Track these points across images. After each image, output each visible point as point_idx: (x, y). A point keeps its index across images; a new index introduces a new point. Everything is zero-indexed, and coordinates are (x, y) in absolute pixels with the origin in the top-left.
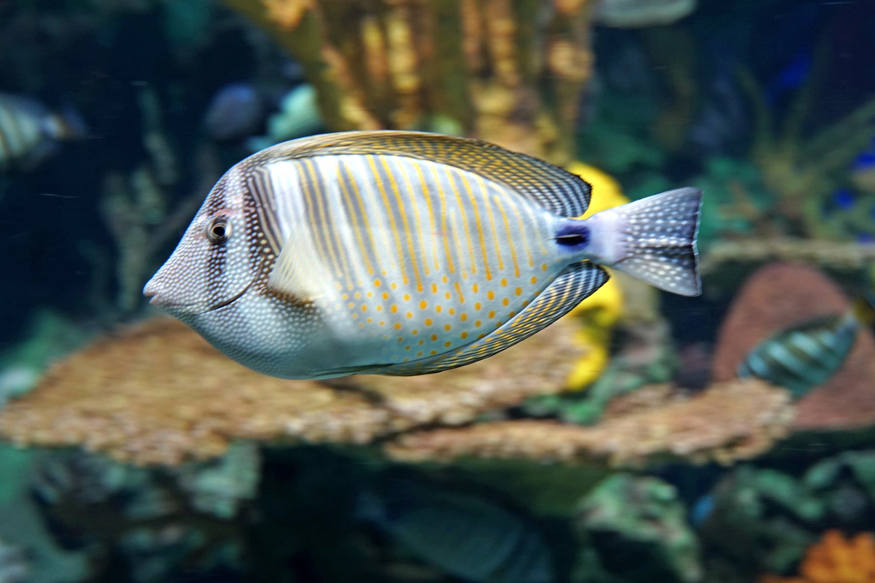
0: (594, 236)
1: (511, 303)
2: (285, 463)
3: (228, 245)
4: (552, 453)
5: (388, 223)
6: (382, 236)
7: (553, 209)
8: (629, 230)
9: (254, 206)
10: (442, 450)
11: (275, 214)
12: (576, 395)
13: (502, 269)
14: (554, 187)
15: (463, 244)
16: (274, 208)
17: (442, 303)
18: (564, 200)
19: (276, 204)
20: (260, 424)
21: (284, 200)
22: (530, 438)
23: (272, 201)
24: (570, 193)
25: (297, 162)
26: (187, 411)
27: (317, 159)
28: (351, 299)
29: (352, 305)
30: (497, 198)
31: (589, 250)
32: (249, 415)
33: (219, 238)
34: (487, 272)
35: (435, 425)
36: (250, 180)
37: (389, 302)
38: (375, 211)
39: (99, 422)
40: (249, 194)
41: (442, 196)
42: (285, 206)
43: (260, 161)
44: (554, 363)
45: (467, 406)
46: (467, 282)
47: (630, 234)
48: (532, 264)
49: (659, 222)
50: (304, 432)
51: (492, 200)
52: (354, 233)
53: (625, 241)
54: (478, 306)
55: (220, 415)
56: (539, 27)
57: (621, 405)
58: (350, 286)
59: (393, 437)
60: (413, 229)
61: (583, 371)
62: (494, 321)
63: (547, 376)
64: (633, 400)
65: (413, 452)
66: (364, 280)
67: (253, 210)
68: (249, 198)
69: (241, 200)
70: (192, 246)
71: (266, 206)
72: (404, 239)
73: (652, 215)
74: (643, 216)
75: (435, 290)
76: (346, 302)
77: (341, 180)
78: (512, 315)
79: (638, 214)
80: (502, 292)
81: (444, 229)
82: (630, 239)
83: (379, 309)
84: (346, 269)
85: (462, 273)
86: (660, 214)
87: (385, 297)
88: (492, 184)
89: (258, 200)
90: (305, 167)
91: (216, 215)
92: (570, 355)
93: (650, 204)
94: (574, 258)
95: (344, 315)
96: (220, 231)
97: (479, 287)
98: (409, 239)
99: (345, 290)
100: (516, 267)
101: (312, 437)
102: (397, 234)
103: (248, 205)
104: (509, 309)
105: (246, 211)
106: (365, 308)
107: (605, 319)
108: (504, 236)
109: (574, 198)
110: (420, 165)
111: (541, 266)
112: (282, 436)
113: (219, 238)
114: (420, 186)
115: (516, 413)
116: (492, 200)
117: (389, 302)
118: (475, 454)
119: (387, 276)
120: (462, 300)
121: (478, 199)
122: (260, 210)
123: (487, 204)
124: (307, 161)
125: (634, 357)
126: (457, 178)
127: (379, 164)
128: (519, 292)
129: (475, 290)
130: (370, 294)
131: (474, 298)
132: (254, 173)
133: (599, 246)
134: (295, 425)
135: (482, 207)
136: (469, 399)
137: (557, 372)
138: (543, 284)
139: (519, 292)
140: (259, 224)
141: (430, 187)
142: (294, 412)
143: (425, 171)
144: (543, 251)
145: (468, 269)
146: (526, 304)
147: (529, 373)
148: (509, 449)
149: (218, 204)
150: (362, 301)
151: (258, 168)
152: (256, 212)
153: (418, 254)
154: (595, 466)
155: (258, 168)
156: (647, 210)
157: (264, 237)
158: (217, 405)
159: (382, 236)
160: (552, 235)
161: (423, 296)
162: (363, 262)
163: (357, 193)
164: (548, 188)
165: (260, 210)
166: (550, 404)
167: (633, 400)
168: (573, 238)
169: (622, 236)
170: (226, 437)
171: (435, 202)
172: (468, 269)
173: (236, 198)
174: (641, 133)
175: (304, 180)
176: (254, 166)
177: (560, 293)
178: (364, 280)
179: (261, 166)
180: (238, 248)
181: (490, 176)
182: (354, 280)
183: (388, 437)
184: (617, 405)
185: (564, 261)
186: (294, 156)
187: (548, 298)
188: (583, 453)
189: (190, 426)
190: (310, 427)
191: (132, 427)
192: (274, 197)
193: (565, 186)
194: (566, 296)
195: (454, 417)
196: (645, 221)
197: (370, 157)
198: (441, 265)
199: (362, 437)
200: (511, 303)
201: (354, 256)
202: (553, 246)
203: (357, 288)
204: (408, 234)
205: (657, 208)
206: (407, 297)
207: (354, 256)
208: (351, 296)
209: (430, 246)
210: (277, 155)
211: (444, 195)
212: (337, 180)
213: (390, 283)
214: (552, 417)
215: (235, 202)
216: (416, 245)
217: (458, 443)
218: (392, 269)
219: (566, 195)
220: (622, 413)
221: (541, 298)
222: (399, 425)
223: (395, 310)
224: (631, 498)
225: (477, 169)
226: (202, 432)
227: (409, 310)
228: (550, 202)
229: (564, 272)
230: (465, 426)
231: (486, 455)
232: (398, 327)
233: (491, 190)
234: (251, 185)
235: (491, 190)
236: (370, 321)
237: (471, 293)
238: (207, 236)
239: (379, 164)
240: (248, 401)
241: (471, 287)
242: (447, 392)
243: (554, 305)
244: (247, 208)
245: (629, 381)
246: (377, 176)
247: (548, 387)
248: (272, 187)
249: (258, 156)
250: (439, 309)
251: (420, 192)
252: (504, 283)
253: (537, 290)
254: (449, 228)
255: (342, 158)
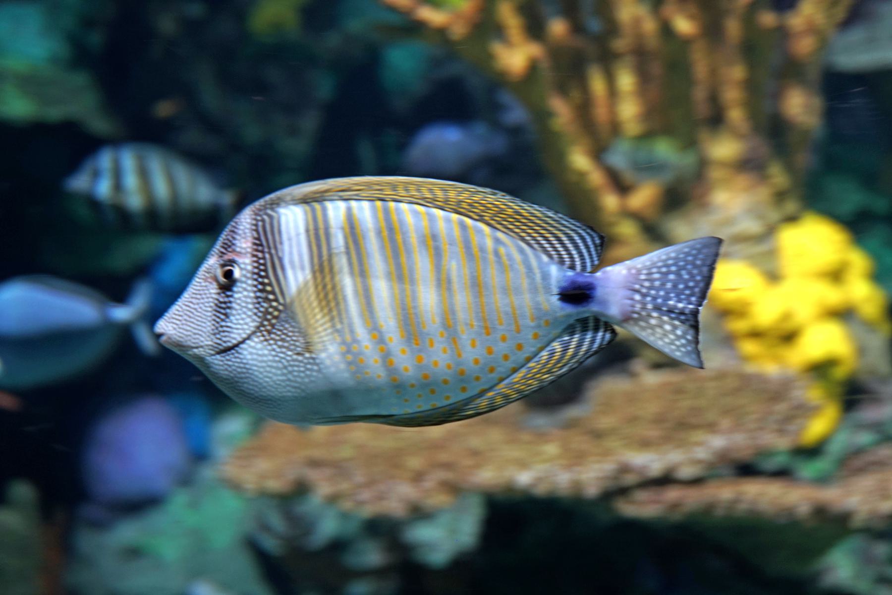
0: (599, 292)
1: (512, 358)
2: (510, 516)
3: (235, 289)
4: (789, 512)
5: (389, 276)
6: (381, 288)
7: (561, 262)
8: (637, 287)
9: (262, 252)
10: (675, 506)
11: (281, 260)
12: (812, 452)
13: (501, 324)
14: (564, 238)
15: (462, 299)
16: (280, 254)
17: (440, 358)
18: (574, 252)
19: (283, 251)
20: (488, 476)
21: (291, 246)
22: (763, 495)
23: (279, 246)
24: (581, 245)
25: (307, 207)
26: (415, 462)
27: (329, 205)
28: (349, 351)
29: (350, 357)
30: (502, 250)
31: (593, 308)
32: (478, 466)
33: (228, 283)
34: (486, 328)
35: (666, 480)
36: (260, 224)
37: (386, 356)
38: (377, 263)
39: (328, 472)
40: (258, 239)
41: (445, 247)
42: (291, 253)
43: (272, 204)
44: (789, 419)
45: (699, 462)
46: (465, 337)
47: (637, 291)
48: (533, 320)
49: (672, 277)
50: (533, 485)
51: (496, 253)
52: (355, 285)
53: (632, 299)
54: (476, 362)
55: (447, 466)
56: (771, 64)
57: (858, 463)
58: (348, 338)
59: (623, 492)
60: (413, 282)
61: (817, 427)
62: (495, 376)
63: (781, 432)
64: (870, 458)
65: (643, 507)
66: (361, 332)
67: (260, 255)
68: (257, 242)
69: (249, 245)
70: (202, 291)
71: (273, 251)
72: (403, 291)
73: (664, 270)
74: (654, 270)
75: (432, 345)
76: (344, 354)
77: (347, 226)
78: (515, 371)
79: (649, 269)
80: (502, 348)
81: (443, 283)
82: (637, 297)
83: (376, 362)
84: (345, 321)
85: (460, 328)
86: (673, 269)
87: (382, 350)
88: (500, 235)
89: (266, 243)
90: (314, 211)
91: (226, 257)
92: (806, 411)
93: (664, 257)
94: (578, 314)
95: (342, 366)
96: (229, 275)
97: (478, 343)
98: (409, 293)
99: (344, 342)
100: (516, 322)
101: (541, 490)
102: (396, 286)
103: (257, 250)
104: (510, 365)
105: (254, 256)
106: (362, 361)
107: (840, 373)
108: (505, 290)
109: (584, 251)
110: (428, 214)
111: (542, 322)
112: (510, 489)
113: (228, 283)
114: (424, 236)
115: (746, 469)
116: (496, 253)
117: (386, 356)
118: (709, 509)
119: (384, 329)
120: (459, 355)
121: (482, 249)
122: (267, 256)
123: (491, 257)
124: (317, 206)
125: (869, 413)
126: (463, 226)
127: (386, 211)
128: (520, 347)
129: (473, 345)
130: (367, 347)
131: (472, 353)
132: (265, 217)
133: (604, 303)
134: (524, 478)
135: (485, 259)
136: (701, 454)
137: (792, 427)
138: (546, 340)
139: (520, 347)
140: (265, 271)
141: (435, 237)
142: (523, 465)
143: (432, 219)
144: (545, 306)
145: (467, 324)
146: (529, 360)
147: (761, 429)
148: (742, 507)
149: (229, 246)
150: (360, 353)
151: (269, 212)
152: (264, 258)
153: (415, 307)
154: (833, 525)
155: (269, 212)
156: (660, 264)
157: (270, 284)
158: (444, 457)
159: (381, 288)
160: (555, 290)
161: (420, 351)
162: (362, 315)
163: (361, 242)
164: (546, 239)
165: (267, 256)
166: (779, 461)
167: (870, 458)
168: (577, 294)
169: (629, 293)
170: (454, 489)
171: (437, 255)
172: (467, 324)
173: (245, 243)
174: (869, 180)
175: (311, 227)
176: (266, 208)
177: (565, 350)
178: (361, 332)
179: (272, 209)
180: (244, 294)
181: (499, 226)
182: (352, 331)
183: (617, 491)
184: (852, 464)
185: (569, 316)
186: (305, 201)
187: (552, 354)
188: (821, 512)
189: (418, 477)
190: (539, 480)
191: (359, 478)
192: (281, 243)
193: (576, 238)
194: (570, 352)
195: (686, 472)
196: (657, 276)
197: (379, 204)
198: (437, 320)
199: (592, 491)
200: (512, 358)
201: (353, 306)
202: (555, 300)
203: (355, 341)
204: (407, 287)
205: (670, 262)
206: (403, 352)
207: (353, 306)
208: (349, 348)
209: (428, 298)
210: (288, 198)
211: (447, 246)
212: (343, 228)
213: (387, 337)
214: (782, 474)
215: (244, 245)
216: (414, 298)
217: (691, 499)
218: (388, 321)
219: (577, 247)
220: (861, 471)
221: (545, 354)
222: (630, 479)
223: (391, 363)
224: (866, 559)
225: (486, 218)
226: (429, 483)
227: (405, 362)
228: (560, 255)
229: (570, 330)
230: (696, 482)
231: (720, 512)
232: (395, 380)
233: (497, 241)
234: (260, 229)
235: (497, 241)
236: (367, 373)
237: (469, 348)
238: (216, 279)
239: (386, 211)
240: (475, 453)
241: (469, 342)
242: (679, 446)
243: (559, 361)
244: (255, 253)
245: (865, 438)
246: (383, 224)
247: (782, 443)
248: (280, 232)
249: (271, 200)
250: (436, 364)
251: (423, 241)
252: (504, 339)
253: (539, 345)
254: (449, 281)
255: (353, 204)
